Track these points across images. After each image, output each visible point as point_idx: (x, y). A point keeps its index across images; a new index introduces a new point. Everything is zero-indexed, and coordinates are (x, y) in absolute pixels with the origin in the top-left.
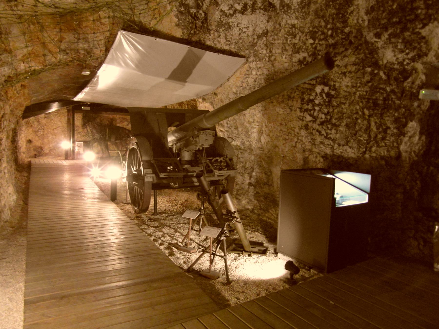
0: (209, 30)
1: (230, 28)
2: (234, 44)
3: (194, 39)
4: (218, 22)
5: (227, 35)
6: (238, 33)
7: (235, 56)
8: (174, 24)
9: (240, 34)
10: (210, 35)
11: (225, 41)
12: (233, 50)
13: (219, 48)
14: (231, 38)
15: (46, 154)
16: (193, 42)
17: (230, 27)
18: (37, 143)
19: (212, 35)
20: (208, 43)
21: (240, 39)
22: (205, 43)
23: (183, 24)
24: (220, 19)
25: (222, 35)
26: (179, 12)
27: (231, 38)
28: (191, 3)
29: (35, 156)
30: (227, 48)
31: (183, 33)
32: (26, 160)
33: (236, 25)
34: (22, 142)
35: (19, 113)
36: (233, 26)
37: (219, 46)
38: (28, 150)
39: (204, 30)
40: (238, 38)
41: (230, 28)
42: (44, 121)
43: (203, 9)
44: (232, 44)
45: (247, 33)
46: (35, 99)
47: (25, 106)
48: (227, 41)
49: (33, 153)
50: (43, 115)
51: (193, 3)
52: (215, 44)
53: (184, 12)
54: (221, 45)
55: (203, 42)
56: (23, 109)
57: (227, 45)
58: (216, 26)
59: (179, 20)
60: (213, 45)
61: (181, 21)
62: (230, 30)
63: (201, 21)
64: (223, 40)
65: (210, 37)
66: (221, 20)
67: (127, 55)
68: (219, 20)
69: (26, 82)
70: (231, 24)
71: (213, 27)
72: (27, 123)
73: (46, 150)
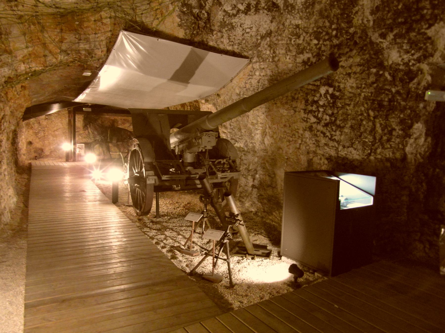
0: (212, 31)
1: (233, 29)
2: (237, 45)
3: (197, 39)
4: (221, 22)
5: (230, 36)
6: (241, 33)
7: (238, 57)
8: (176, 25)
9: (243, 35)
10: (213, 36)
11: (228, 41)
12: (237, 51)
13: (222, 48)
14: (234, 39)
15: (47, 156)
16: (196, 42)
17: (233, 27)
18: (38, 144)
19: (215, 36)
20: (211, 44)
21: (243, 39)
22: (208, 43)
23: (185, 24)
24: (223, 19)
25: (225, 35)
26: (182, 12)
27: (234, 39)
28: (193, 3)
29: (36, 158)
30: (230, 48)
31: (185, 33)
32: (27, 162)
33: (239, 26)
34: (22, 144)
35: (20, 114)
36: (236, 26)
37: (221, 47)
38: (29, 152)
39: (207, 30)
40: (241, 39)
41: (233, 29)
42: (44, 123)
43: (205, 9)
44: (235, 44)
45: (250, 33)
46: (35, 100)
47: (25, 107)
48: (230, 41)
49: (34, 155)
50: (43, 117)
51: (195, 3)
52: (218, 45)
53: (186, 12)
54: (224, 45)
55: (206, 42)
56: (23, 110)
57: (230, 45)
58: (219, 26)
59: (181, 20)
60: (216, 46)
61: (183, 22)
62: (233, 30)
63: (204, 21)
64: (226, 41)
65: (213, 38)
66: (224, 20)
67: (128, 56)
68: (222, 20)
69: (26, 83)
70: (234, 24)
71: (216, 28)
72: (28, 125)
73: (47, 152)
